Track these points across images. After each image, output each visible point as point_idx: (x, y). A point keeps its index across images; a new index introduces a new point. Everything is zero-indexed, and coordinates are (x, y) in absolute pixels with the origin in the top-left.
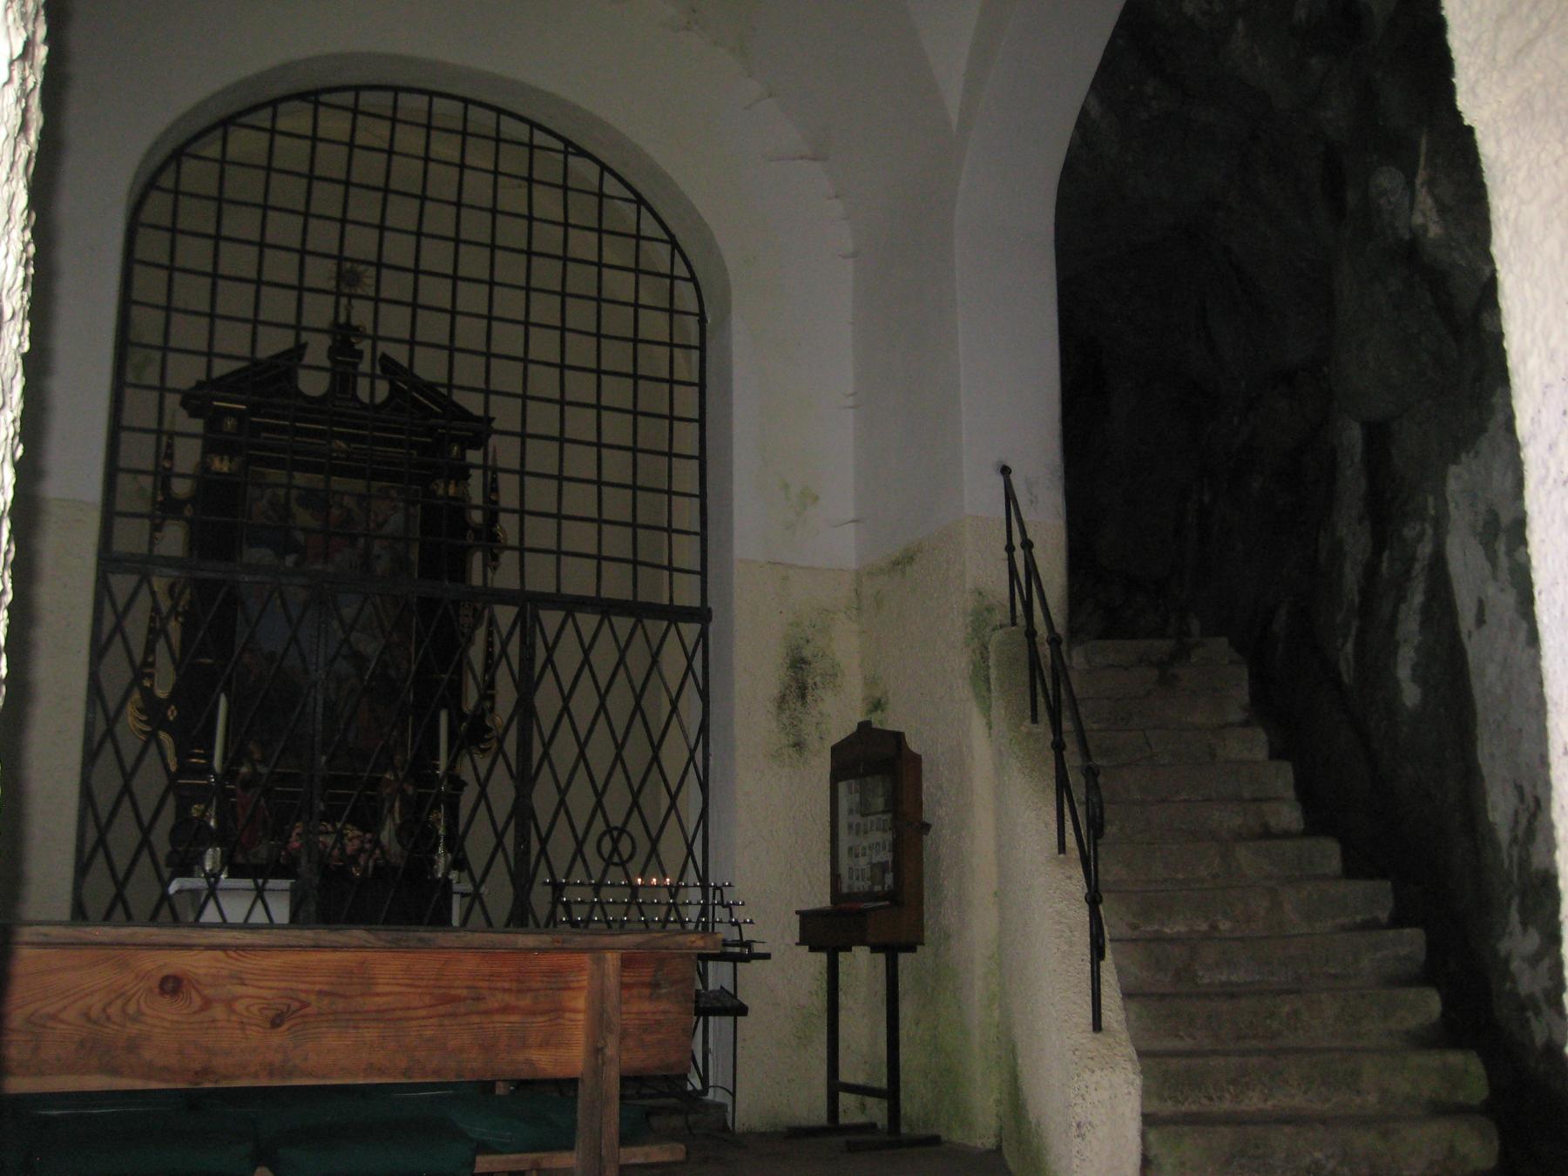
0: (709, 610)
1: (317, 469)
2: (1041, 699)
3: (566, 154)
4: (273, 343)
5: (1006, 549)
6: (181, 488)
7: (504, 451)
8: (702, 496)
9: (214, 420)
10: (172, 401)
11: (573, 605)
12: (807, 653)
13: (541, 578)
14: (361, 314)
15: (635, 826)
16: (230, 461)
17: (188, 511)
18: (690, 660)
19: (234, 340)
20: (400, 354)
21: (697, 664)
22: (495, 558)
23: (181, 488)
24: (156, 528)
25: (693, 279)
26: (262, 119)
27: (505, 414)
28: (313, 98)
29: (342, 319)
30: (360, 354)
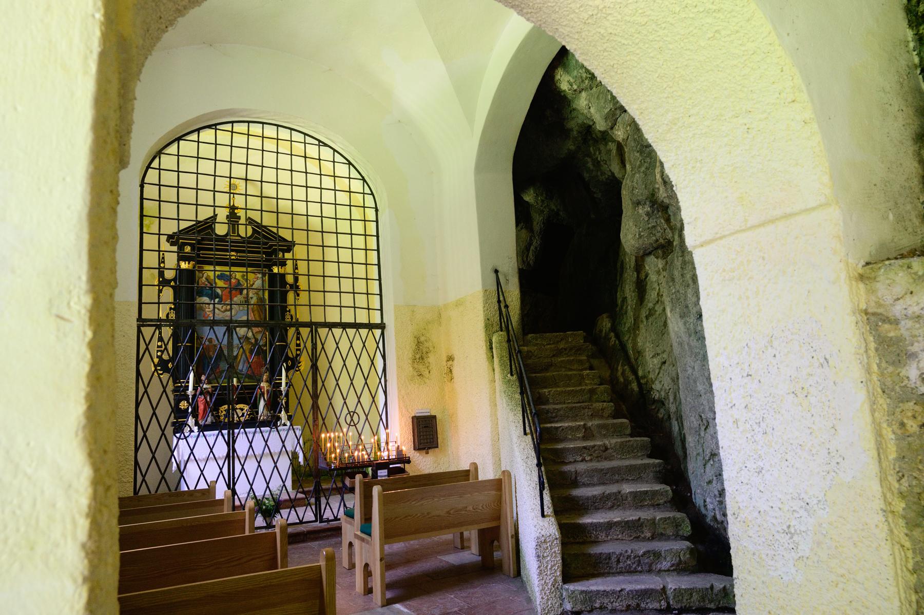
0: (385, 324)
1: (225, 264)
2: (503, 323)
3: (319, 146)
4: (205, 214)
5: (537, 465)
6: (169, 275)
7: (299, 252)
8: (380, 280)
9: (181, 248)
10: (164, 239)
11: (331, 326)
12: (422, 339)
13: (318, 317)
14: (239, 201)
15: (359, 410)
16: (189, 264)
17: (173, 283)
18: (378, 344)
19: (188, 213)
20: (256, 216)
21: (143, 347)
22: (298, 295)
23: (169, 275)
24: (160, 291)
25: (372, 194)
26: (194, 137)
27: (299, 237)
28: (214, 127)
29: (232, 204)
30: (239, 218)
